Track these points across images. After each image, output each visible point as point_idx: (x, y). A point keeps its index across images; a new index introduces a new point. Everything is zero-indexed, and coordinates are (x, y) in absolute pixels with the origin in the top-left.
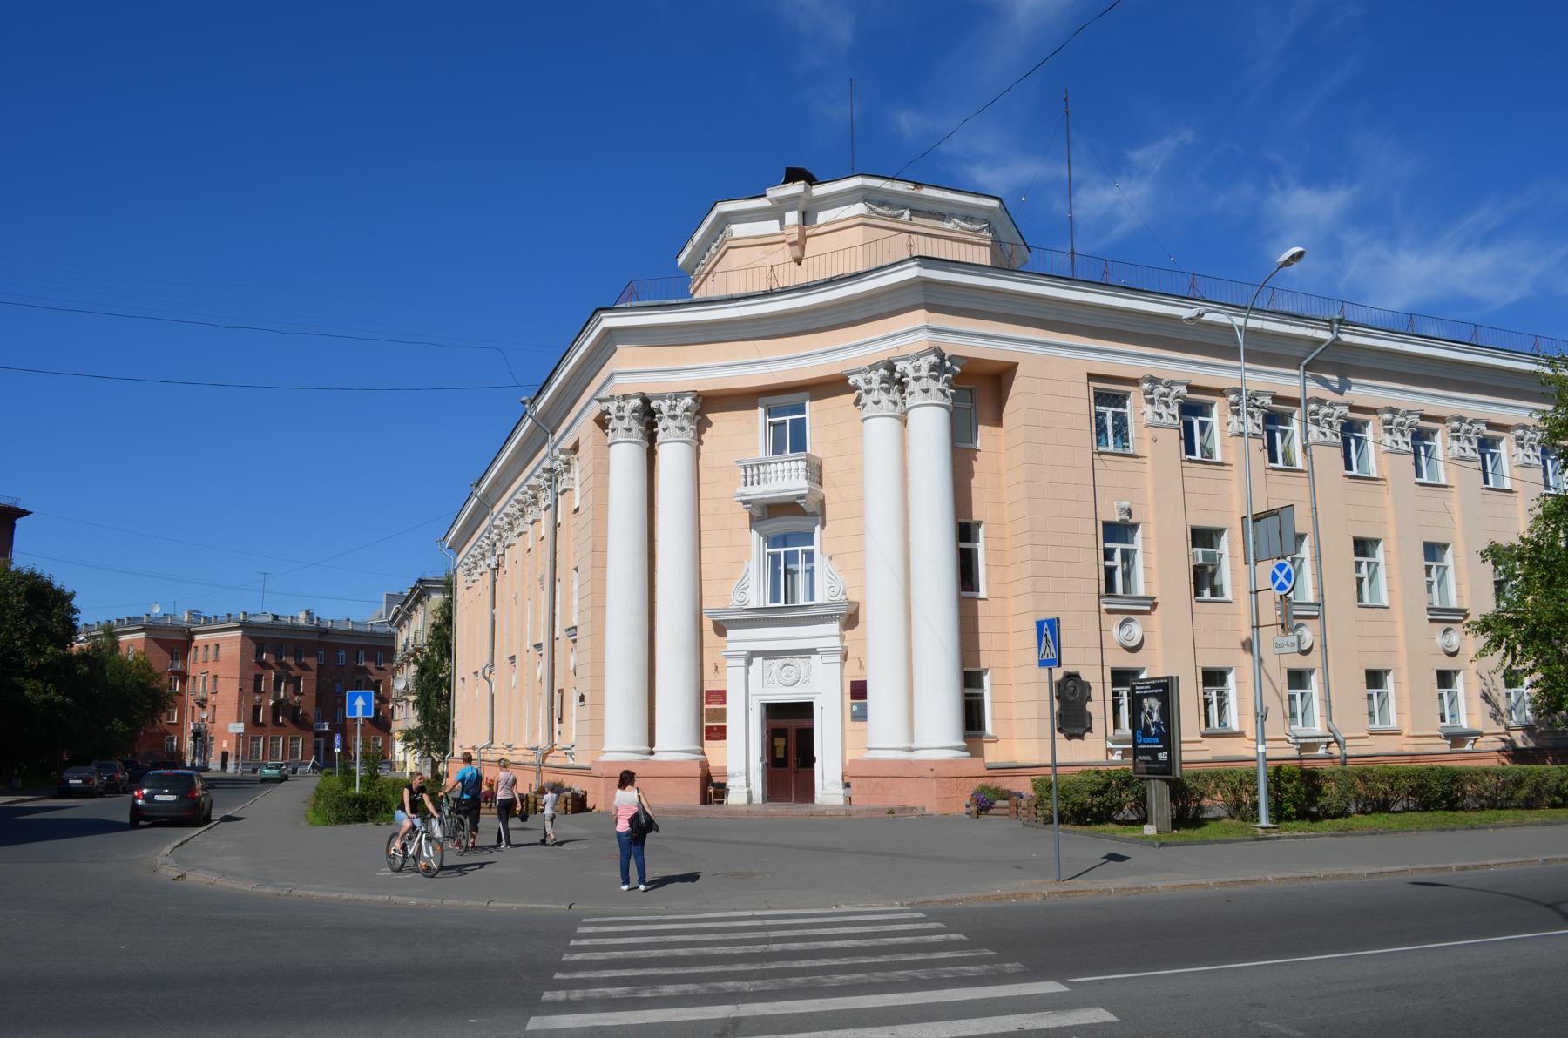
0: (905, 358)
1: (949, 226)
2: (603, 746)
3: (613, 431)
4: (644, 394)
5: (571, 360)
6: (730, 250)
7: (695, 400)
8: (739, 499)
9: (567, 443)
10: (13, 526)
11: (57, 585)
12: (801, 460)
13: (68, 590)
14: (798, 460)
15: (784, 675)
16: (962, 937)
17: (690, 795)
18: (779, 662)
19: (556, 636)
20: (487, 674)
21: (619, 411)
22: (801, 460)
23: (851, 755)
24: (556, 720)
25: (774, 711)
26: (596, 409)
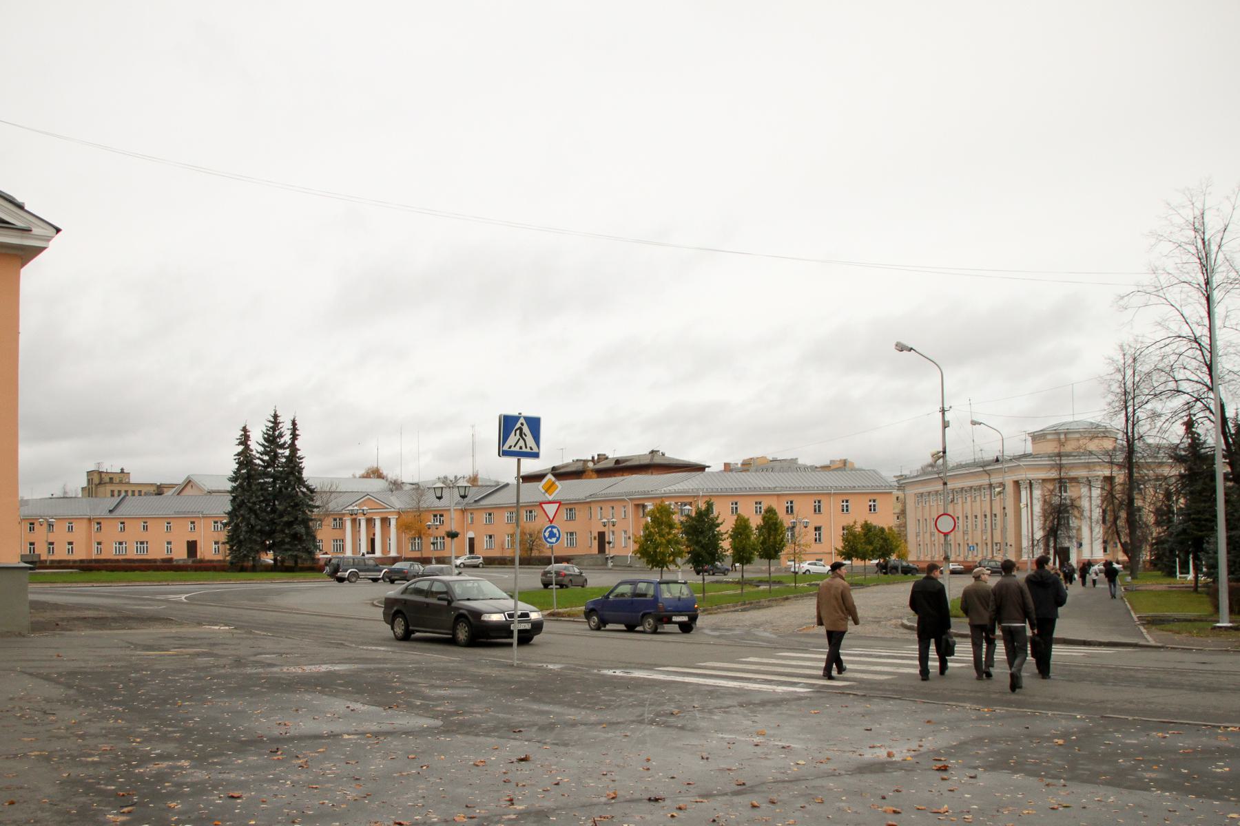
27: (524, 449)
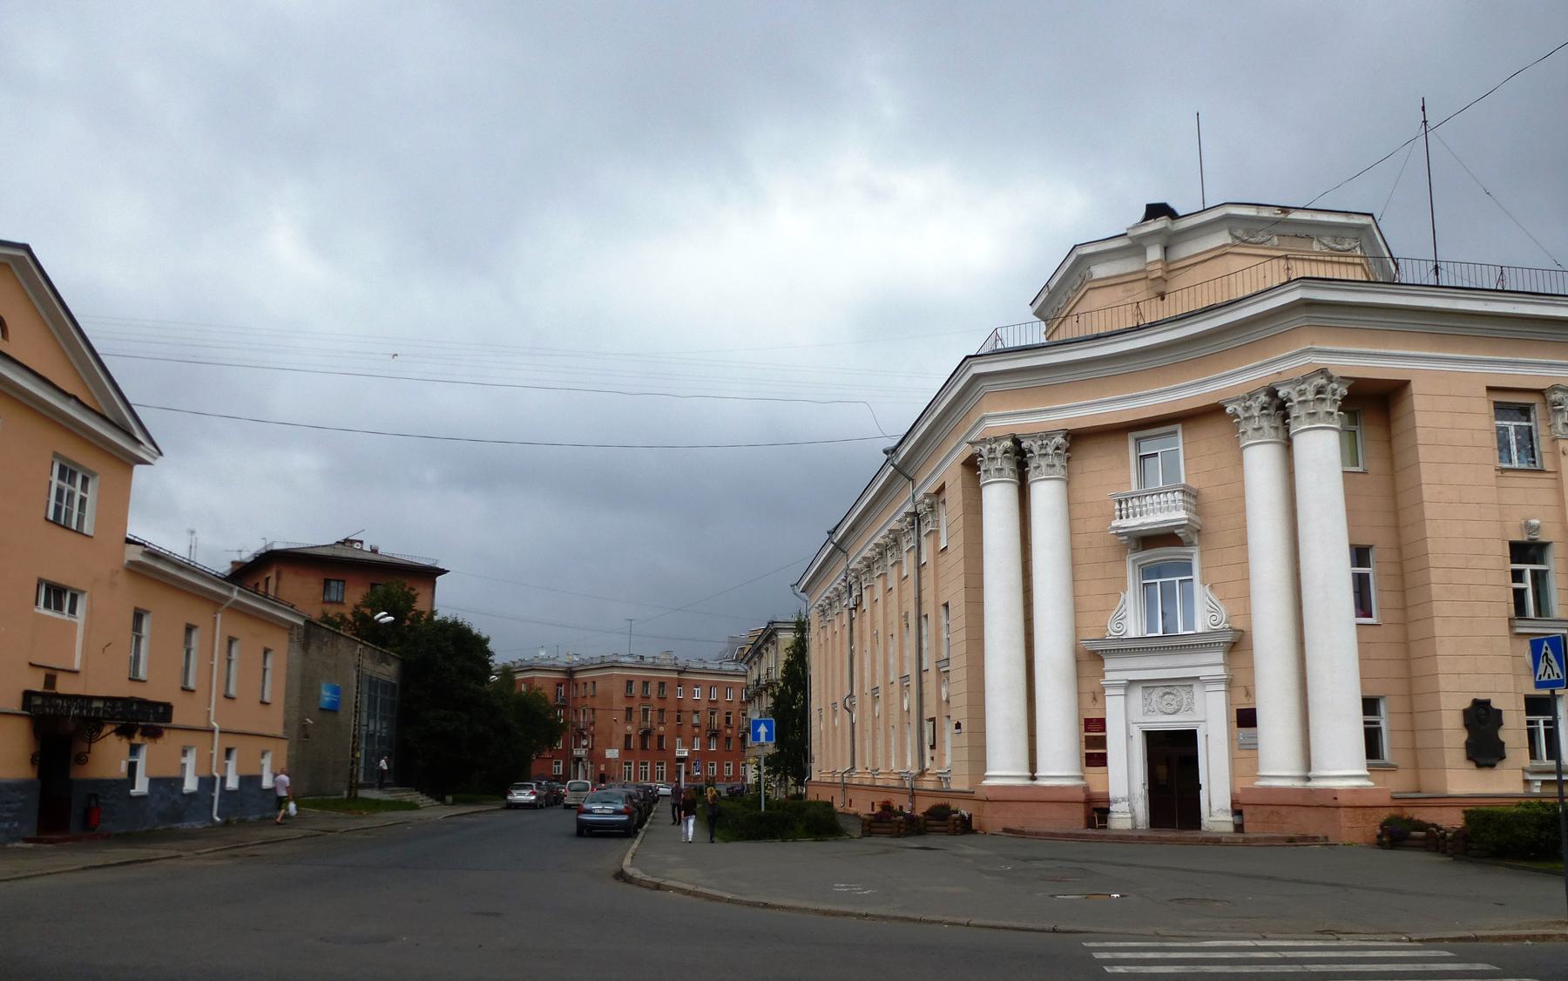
0: (1288, 382)
1: (1316, 247)
2: (1257, 770)
3: (985, 471)
4: (1015, 435)
5: (936, 408)
6: (1089, 292)
7: (1065, 438)
8: (1114, 532)
9: (931, 487)
10: (434, 582)
11: (475, 631)
12: (1178, 491)
13: (484, 636)
14: (1175, 491)
15: (1164, 703)
16: (1085, 944)
17: (1075, 820)
18: (1159, 692)
19: (924, 668)
20: (848, 705)
21: (990, 453)
22: (1178, 491)
23: (1244, 783)
24: (927, 748)
25: (1155, 741)
26: (965, 451)
27: (1552, 678)
